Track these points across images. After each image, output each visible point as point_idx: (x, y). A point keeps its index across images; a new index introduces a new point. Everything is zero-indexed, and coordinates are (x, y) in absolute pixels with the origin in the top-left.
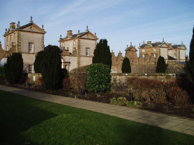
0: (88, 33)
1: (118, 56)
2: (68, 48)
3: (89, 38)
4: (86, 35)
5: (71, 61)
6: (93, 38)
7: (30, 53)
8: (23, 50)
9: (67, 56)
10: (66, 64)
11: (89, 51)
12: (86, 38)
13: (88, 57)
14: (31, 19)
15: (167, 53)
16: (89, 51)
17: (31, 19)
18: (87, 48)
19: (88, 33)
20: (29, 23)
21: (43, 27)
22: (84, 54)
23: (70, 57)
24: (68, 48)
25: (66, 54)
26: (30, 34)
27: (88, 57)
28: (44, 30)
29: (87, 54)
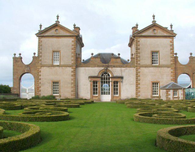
0: (154, 26)
1: (89, 60)
2: (20, 54)
3: (158, 34)
4: (151, 30)
5: (124, 75)
6: (165, 34)
7: (53, 66)
8: (45, 62)
9: (117, 67)
10: (116, 80)
11: (158, 57)
12: (152, 34)
13: (155, 66)
14: (154, 19)
15: (169, 48)
16: (158, 57)
17: (154, 19)
18: (153, 53)
19: (154, 26)
20: (152, 23)
21: (171, 28)
22: (149, 62)
23: (123, 69)
24: (20, 54)
25: (117, 64)
26: (55, 40)
27: (155, 66)
28: (173, 31)
29: (153, 61)
